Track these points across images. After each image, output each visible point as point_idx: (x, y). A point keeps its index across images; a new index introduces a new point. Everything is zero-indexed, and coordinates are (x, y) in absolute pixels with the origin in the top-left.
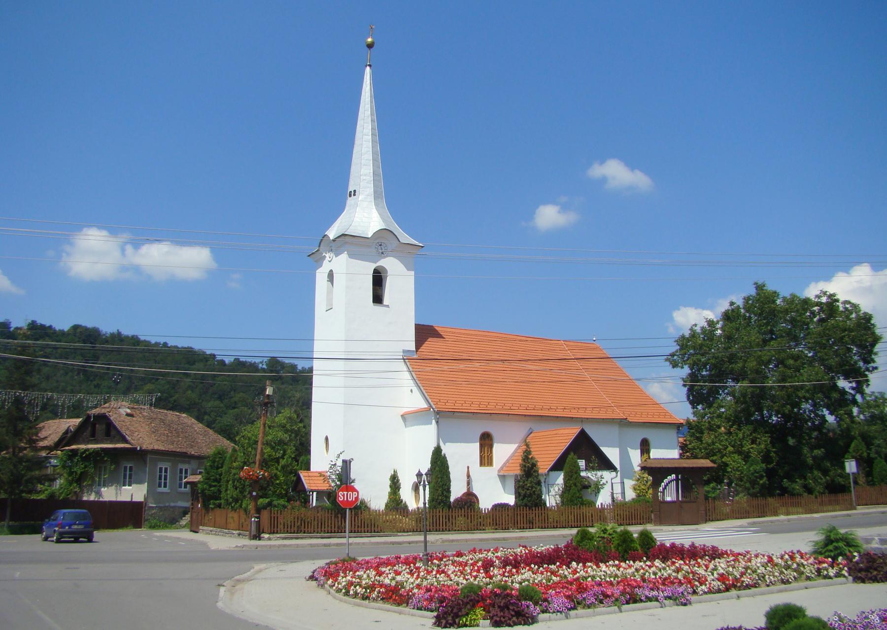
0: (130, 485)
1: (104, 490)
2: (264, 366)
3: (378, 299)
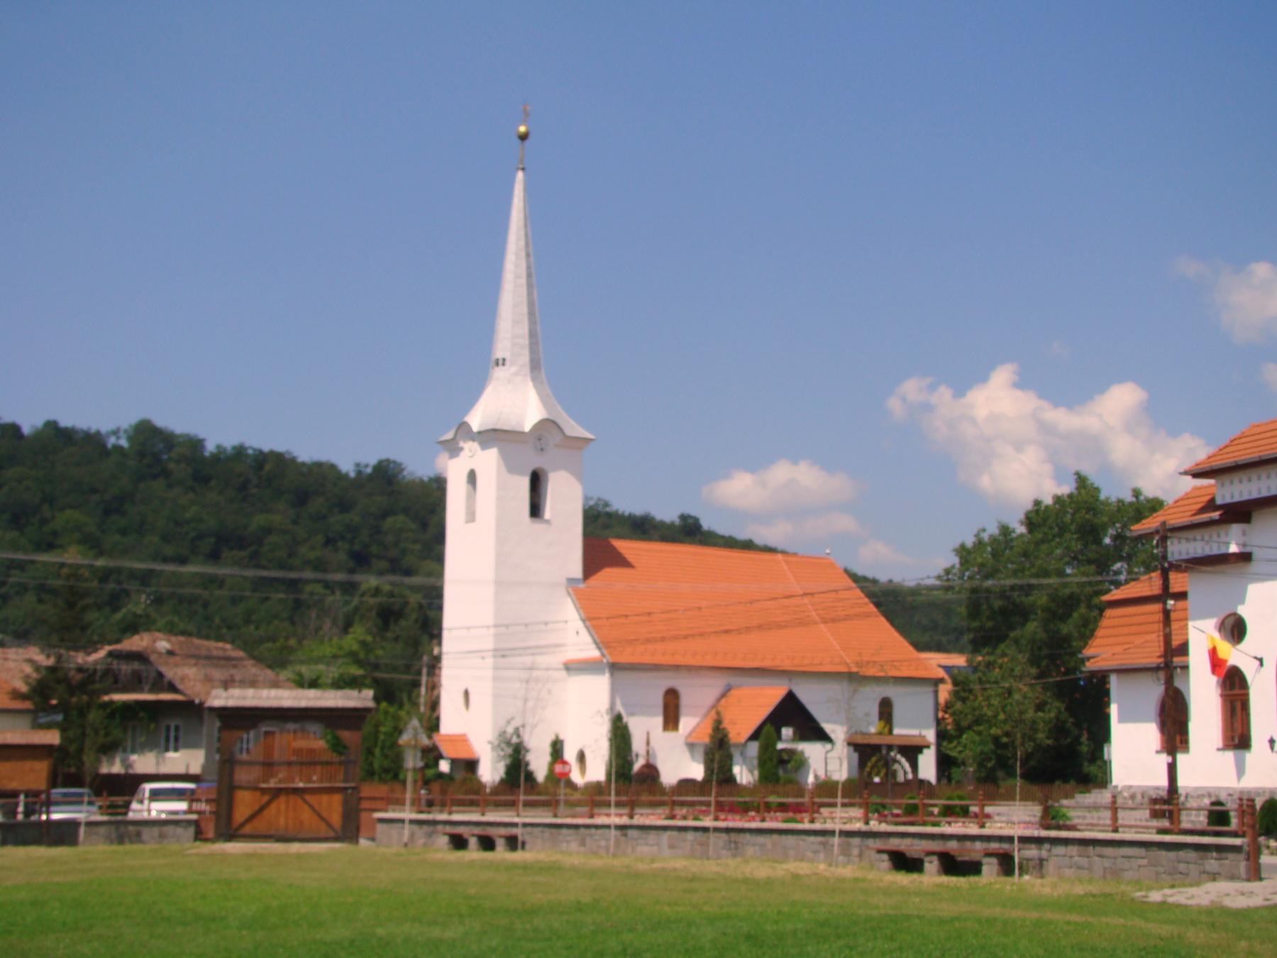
0: (176, 750)
1: (134, 757)
2: (124, 443)
3: (536, 510)
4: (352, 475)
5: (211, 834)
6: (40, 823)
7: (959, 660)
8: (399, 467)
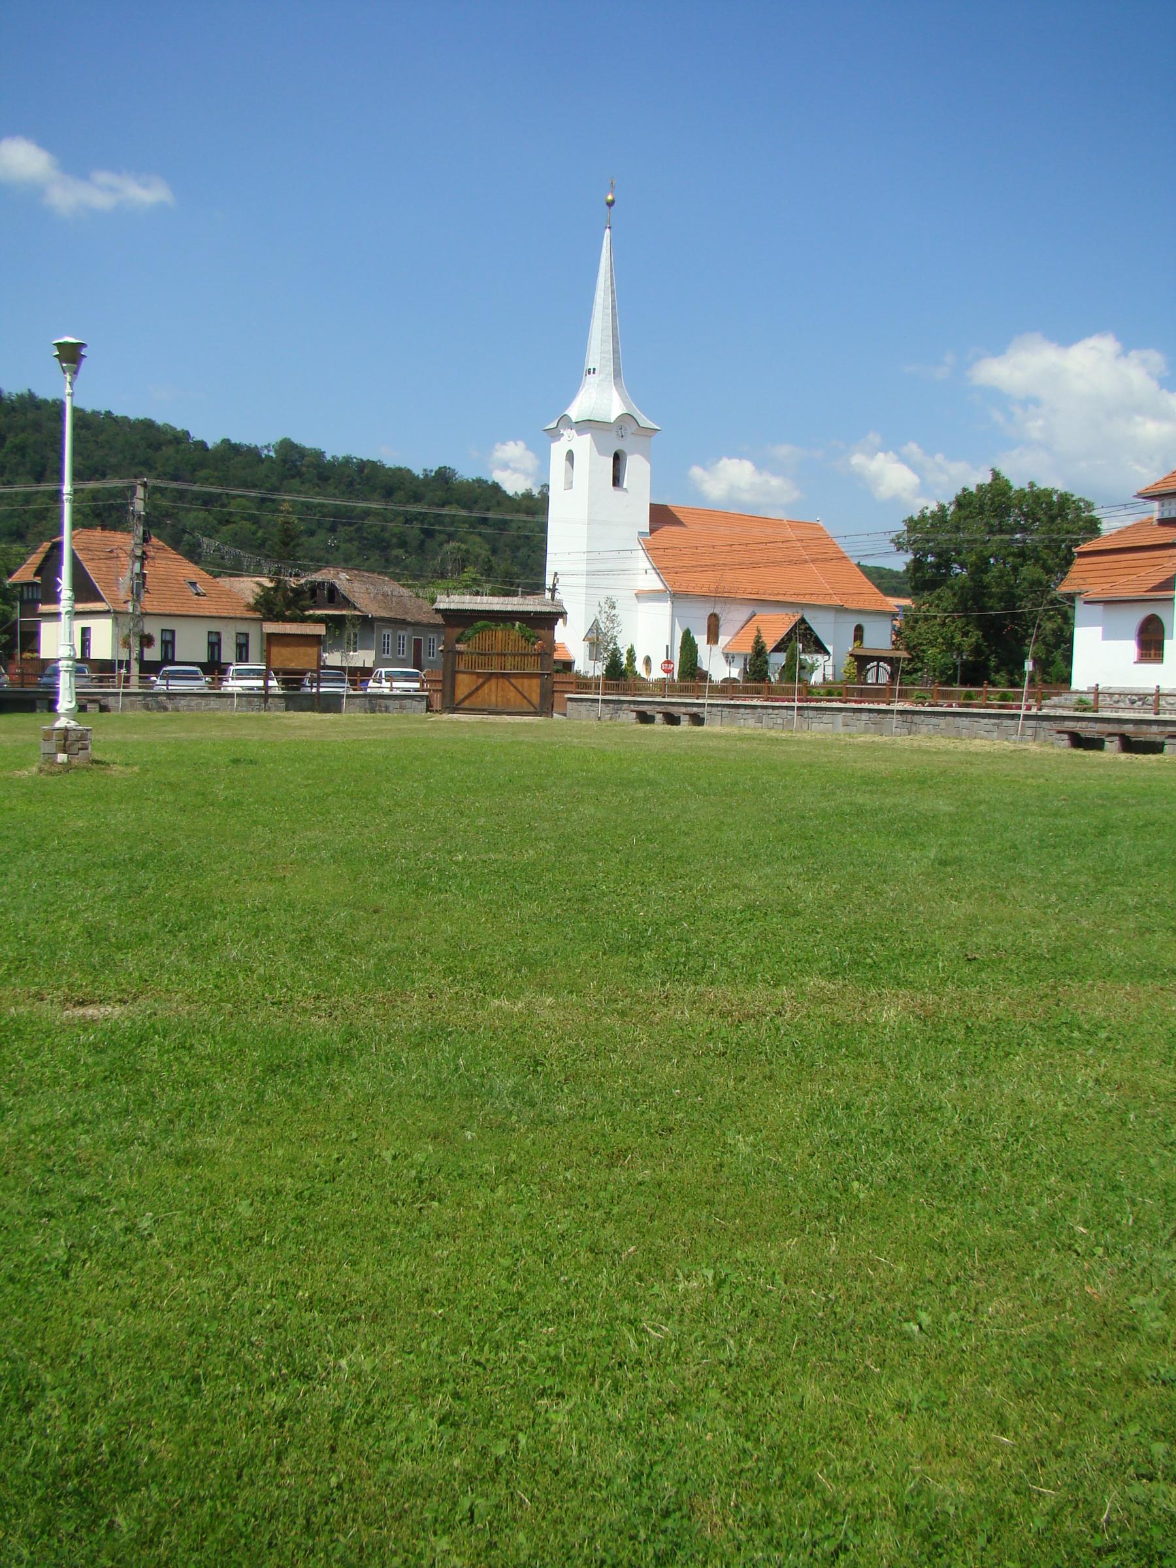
0: (355, 651)
2: (272, 454)
3: (617, 481)
4: (422, 477)
5: (437, 705)
6: (312, 695)
7: (906, 602)
8: (454, 472)
